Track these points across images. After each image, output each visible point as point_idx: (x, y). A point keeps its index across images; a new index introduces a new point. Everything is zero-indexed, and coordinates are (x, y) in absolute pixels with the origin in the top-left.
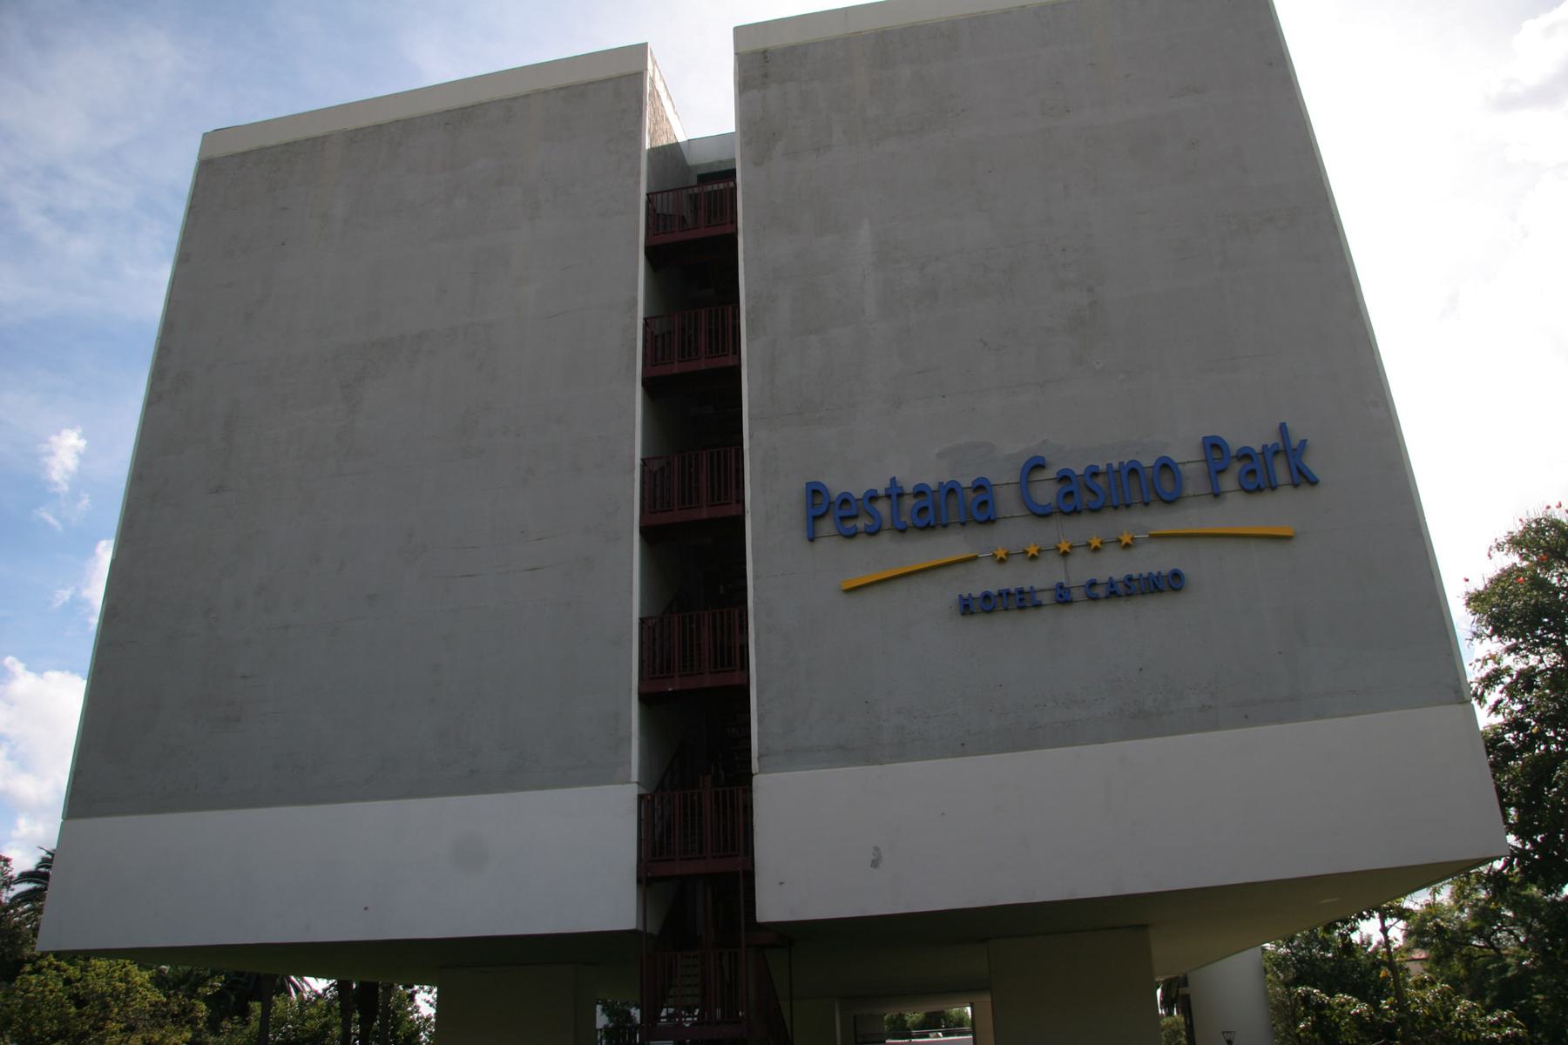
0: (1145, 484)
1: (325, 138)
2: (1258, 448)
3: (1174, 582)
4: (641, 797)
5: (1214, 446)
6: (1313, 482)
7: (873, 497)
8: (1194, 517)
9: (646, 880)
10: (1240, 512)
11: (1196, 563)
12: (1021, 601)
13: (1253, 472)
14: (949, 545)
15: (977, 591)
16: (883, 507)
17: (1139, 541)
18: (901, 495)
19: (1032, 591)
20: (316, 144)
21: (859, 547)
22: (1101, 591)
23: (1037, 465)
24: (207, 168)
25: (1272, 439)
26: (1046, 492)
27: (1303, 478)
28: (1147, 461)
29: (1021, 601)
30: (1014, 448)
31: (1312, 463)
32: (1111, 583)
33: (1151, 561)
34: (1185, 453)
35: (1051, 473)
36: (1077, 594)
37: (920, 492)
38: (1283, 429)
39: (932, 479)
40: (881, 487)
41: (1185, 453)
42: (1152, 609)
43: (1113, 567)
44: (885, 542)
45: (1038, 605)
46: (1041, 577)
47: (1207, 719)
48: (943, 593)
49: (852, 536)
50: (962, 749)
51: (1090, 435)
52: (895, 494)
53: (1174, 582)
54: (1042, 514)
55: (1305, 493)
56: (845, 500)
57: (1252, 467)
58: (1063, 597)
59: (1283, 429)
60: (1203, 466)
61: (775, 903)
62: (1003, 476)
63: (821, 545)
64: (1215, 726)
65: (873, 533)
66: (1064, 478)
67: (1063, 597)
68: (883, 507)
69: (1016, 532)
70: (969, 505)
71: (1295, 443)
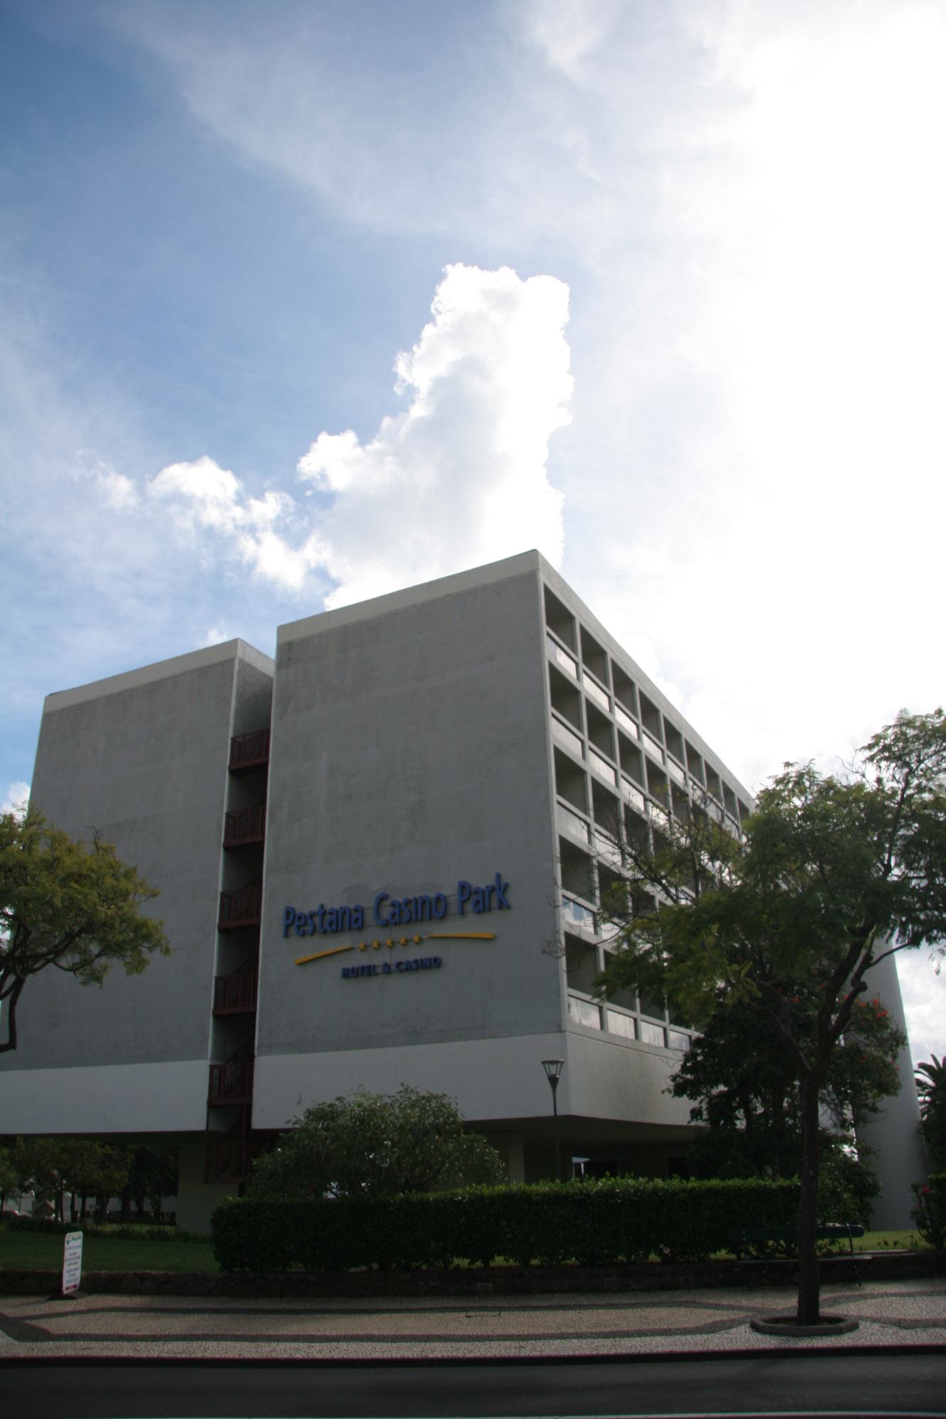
0: (427, 909)
3: (435, 963)
4: (212, 1067)
5: (463, 887)
6: (509, 908)
7: (312, 915)
9: (212, 1106)
10: (471, 925)
12: (368, 971)
19: (375, 966)
22: (403, 967)
25: (491, 881)
26: (386, 912)
29: (368, 971)
34: (451, 891)
36: (393, 968)
38: (499, 876)
40: (315, 908)
41: (451, 891)
42: (426, 977)
43: (413, 954)
44: (317, 939)
46: (378, 959)
47: (443, 1036)
49: (304, 934)
52: (323, 912)
53: (435, 963)
54: (386, 924)
58: (387, 969)
59: (499, 876)
61: (260, 1121)
62: (369, 903)
65: (313, 933)
67: (387, 969)
70: (343, 921)
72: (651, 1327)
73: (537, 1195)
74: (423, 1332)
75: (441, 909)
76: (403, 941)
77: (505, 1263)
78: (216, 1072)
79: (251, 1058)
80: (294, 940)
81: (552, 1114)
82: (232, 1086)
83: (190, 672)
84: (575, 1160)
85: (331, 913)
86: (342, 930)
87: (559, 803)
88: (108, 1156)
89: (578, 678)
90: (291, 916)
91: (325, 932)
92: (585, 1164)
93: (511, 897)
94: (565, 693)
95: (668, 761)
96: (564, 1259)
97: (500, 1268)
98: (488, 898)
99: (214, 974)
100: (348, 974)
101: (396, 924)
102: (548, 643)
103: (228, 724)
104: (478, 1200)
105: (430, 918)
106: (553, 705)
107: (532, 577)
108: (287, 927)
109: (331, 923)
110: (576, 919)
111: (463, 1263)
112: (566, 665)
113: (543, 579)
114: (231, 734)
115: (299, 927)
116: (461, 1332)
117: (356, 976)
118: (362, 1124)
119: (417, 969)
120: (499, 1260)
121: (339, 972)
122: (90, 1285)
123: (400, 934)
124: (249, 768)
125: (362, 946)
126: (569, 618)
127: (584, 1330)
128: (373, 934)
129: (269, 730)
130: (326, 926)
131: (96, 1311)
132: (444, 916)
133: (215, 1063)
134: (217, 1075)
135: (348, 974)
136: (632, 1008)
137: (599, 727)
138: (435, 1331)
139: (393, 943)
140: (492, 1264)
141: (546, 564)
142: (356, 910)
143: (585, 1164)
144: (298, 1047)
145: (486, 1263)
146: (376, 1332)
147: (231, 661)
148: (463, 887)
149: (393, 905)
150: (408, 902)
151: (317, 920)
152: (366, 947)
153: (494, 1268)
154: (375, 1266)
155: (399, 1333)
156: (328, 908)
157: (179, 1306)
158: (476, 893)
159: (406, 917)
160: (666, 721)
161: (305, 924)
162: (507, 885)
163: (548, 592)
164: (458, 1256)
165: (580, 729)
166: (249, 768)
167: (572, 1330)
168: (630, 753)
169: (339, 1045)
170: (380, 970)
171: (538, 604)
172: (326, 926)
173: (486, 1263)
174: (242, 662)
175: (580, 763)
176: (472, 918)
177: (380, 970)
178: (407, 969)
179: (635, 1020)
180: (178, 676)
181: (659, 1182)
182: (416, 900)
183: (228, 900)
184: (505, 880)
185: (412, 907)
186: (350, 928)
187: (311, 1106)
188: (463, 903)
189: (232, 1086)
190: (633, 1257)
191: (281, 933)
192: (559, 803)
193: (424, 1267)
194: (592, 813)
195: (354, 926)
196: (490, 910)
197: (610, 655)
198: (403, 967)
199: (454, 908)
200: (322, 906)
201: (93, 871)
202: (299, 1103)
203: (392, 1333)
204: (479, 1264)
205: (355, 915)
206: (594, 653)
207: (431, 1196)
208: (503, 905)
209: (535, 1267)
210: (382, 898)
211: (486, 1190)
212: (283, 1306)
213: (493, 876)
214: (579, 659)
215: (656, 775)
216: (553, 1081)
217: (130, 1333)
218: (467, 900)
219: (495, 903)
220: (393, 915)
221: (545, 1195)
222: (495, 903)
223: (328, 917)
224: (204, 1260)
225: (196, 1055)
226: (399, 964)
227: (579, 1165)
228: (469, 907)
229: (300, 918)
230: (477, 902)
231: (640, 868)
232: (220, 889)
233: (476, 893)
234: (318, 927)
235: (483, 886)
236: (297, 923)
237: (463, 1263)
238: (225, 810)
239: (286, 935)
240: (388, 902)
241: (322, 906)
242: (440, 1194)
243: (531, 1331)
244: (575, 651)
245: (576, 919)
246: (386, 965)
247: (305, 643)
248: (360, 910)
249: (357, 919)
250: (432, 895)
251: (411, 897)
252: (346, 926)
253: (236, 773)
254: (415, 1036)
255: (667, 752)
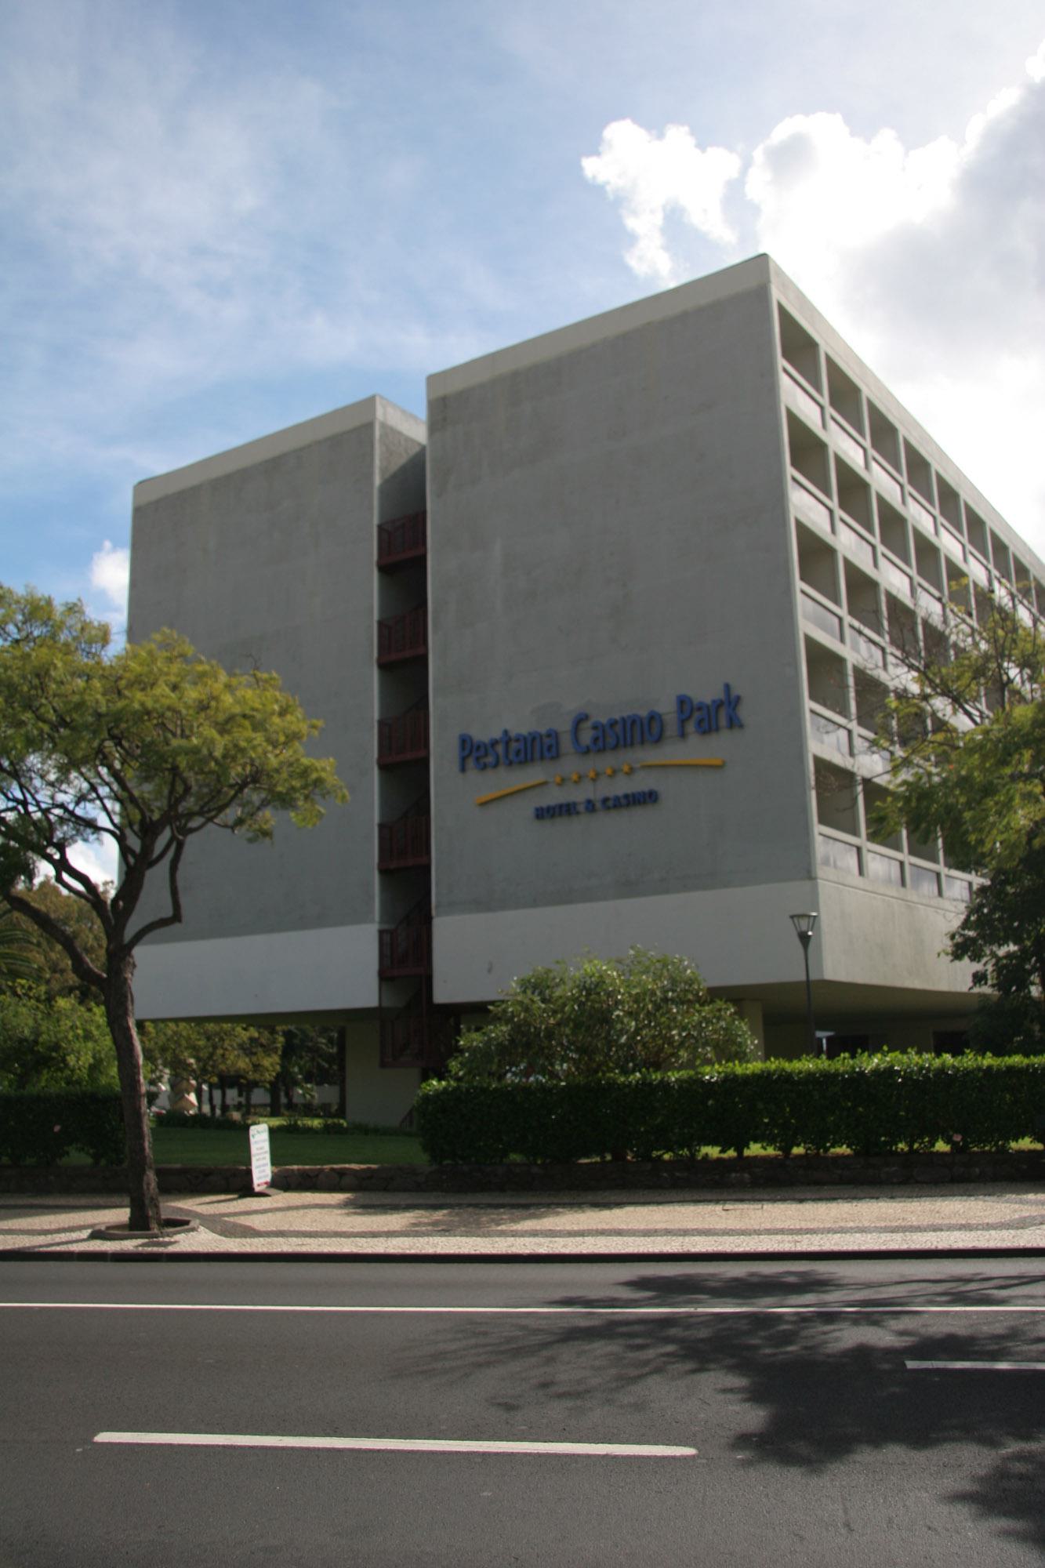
0: (636, 731)
1: (285, 455)
3: (649, 798)
4: (381, 932)
5: (683, 701)
6: (741, 726)
7: (494, 743)
8: (672, 752)
9: (384, 976)
10: (695, 749)
12: (567, 810)
14: (533, 774)
19: (575, 804)
20: (195, 490)
21: (490, 774)
22: (610, 803)
24: (139, 512)
25: (720, 695)
26: (587, 736)
29: (567, 810)
30: (572, 706)
32: (617, 799)
34: (667, 707)
36: (598, 805)
38: (727, 687)
40: (497, 734)
41: (667, 707)
42: (639, 816)
43: (622, 787)
44: (502, 771)
45: (578, 813)
46: (578, 795)
47: (663, 887)
48: (526, 807)
49: (484, 767)
50: (535, 903)
51: (612, 696)
52: (507, 739)
53: (649, 798)
54: (587, 751)
58: (590, 806)
59: (727, 687)
61: (443, 993)
62: (564, 726)
64: (667, 891)
65: (496, 765)
67: (590, 806)
70: (532, 749)
72: (947, 1222)
73: (800, 1072)
74: (677, 1226)
75: (655, 730)
76: (609, 771)
77: (762, 1152)
78: (387, 938)
79: (428, 920)
80: (473, 774)
81: (803, 978)
82: (407, 953)
83: (319, 443)
84: (819, 1034)
85: (517, 740)
86: (532, 760)
87: (803, 592)
88: (252, 1039)
89: (867, 466)
90: (468, 746)
91: (511, 763)
92: (829, 1039)
93: (744, 713)
94: (809, 451)
95: (942, 531)
96: (833, 1146)
97: (755, 1158)
98: (715, 715)
99: (376, 819)
100: (542, 814)
101: (599, 751)
102: (785, 381)
103: (371, 508)
104: (730, 1080)
105: (642, 742)
106: (794, 464)
107: (762, 293)
108: (463, 760)
109: (518, 753)
110: (831, 738)
111: (713, 1151)
112: (809, 412)
113: (776, 294)
114: (376, 521)
115: (477, 759)
116: (721, 1225)
117: (553, 816)
118: (589, 994)
119: (628, 805)
120: (755, 1149)
121: (530, 812)
122: (282, 1182)
123: (606, 762)
124: (403, 559)
125: (558, 779)
126: (811, 345)
127: (867, 1224)
128: (570, 764)
129: (424, 512)
130: (512, 756)
131: (297, 1208)
132: (659, 739)
133: (386, 927)
134: (387, 941)
135: (542, 814)
136: (897, 847)
137: (852, 492)
138: (690, 1226)
139: (597, 774)
140: (747, 1153)
141: (780, 273)
142: (549, 736)
143: (829, 1039)
144: (484, 903)
145: (740, 1151)
146: (623, 1226)
147: (370, 426)
148: (683, 701)
149: (595, 727)
150: (613, 724)
151: (500, 749)
152: (563, 780)
153: (748, 1157)
154: (609, 1157)
155: (651, 1227)
156: (513, 734)
157: (386, 1201)
158: (699, 709)
159: (611, 741)
160: (940, 478)
161: (486, 755)
162: (738, 698)
163: (784, 313)
164: (707, 1144)
165: (871, 530)
166: (403, 559)
167: (851, 1224)
168: (893, 525)
169: (537, 901)
170: (581, 808)
171: (770, 329)
172: (512, 756)
173: (740, 1151)
174: (384, 425)
175: (828, 538)
176: (694, 739)
177: (581, 808)
178: (615, 806)
179: (859, 849)
180: (302, 449)
181: (947, 1058)
182: (623, 720)
183: (387, 729)
184: (735, 692)
185: (618, 728)
186: (542, 758)
187: (527, 974)
188: (683, 722)
189: (407, 953)
190: (916, 1146)
191: (456, 767)
192: (803, 592)
193: (666, 1157)
194: (887, 637)
195: (546, 753)
196: (717, 729)
197: (902, 432)
198: (610, 803)
199: (671, 729)
200: (506, 732)
201: (256, 710)
202: (489, 971)
203: (642, 1227)
204: (731, 1153)
205: (547, 741)
206: (845, 395)
207: (673, 1076)
208: (734, 723)
209: (799, 1156)
210: (580, 720)
211: (739, 1069)
212: (507, 1200)
213: (721, 687)
214: (825, 400)
215: (927, 552)
216: (804, 939)
217: (344, 1229)
218: (689, 717)
219: (723, 721)
220: (595, 740)
221: (810, 1074)
222: (723, 721)
223: (514, 745)
224: (413, 1154)
225: (372, 921)
226: (605, 800)
227: (820, 1040)
228: (691, 727)
229: (479, 747)
230: (700, 722)
231: (931, 681)
232: (376, 716)
233: (699, 709)
234: (502, 759)
235: (708, 700)
236: (475, 754)
237: (713, 1151)
238: (376, 617)
239: (463, 769)
240: (588, 724)
241: (506, 732)
242: (684, 1074)
243: (804, 1225)
244: (819, 389)
245: (831, 738)
246: (589, 802)
247: (463, 396)
248: (553, 735)
249: (549, 748)
250: (644, 713)
251: (617, 716)
252: (537, 755)
253: (386, 569)
254: (629, 887)
255: (908, 488)
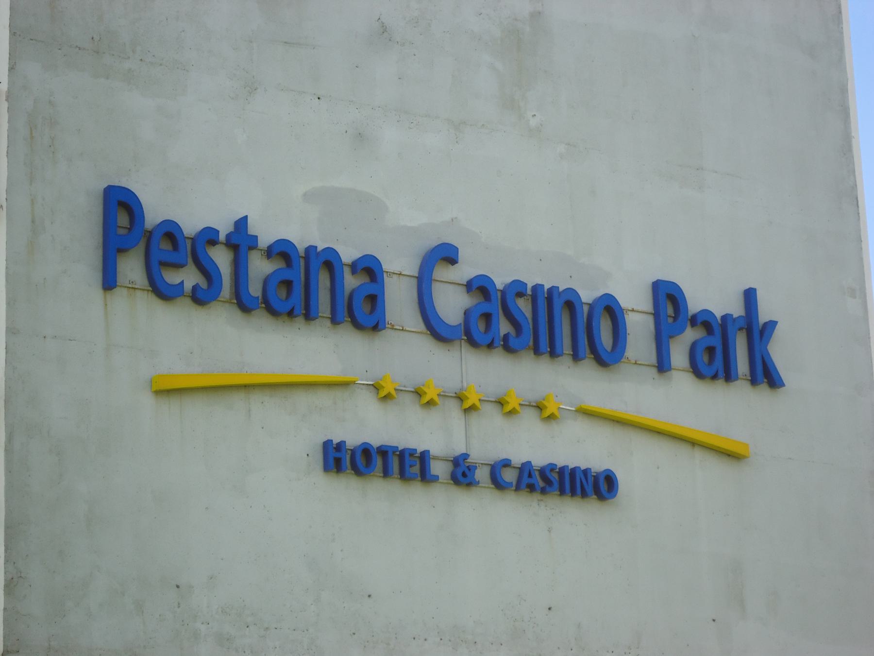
2: (301, 247)
5: (667, 298)
7: (209, 236)
8: (632, 390)
11: (637, 466)
12: (403, 465)
13: (288, 284)
15: (353, 438)
16: (221, 258)
17: (557, 411)
18: (252, 243)
22: (509, 476)
23: (446, 255)
25: (737, 310)
27: (766, 375)
28: (587, 296)
29: (403, 465)
31: (779, 351)
33: (576, 447)
35: (465, 271)
37: (281, 251)
38: (750, 296)
39: (303, 231)
42: (573, 516)
43: (533, 444)
45: (425, 476)
46: (434, 434)
48: (299, 431)
55: (761, 396)
56: (170, 232)
57: (288, 275)
58: (462, 473)
59: (750, 296)
60: (650, 321)
63: (119, 297)
65: (199, 298)
66: (480, 287)
67: (462, 473)
68: (221, 258)
69: (405, 353)
71: (764, 316)
